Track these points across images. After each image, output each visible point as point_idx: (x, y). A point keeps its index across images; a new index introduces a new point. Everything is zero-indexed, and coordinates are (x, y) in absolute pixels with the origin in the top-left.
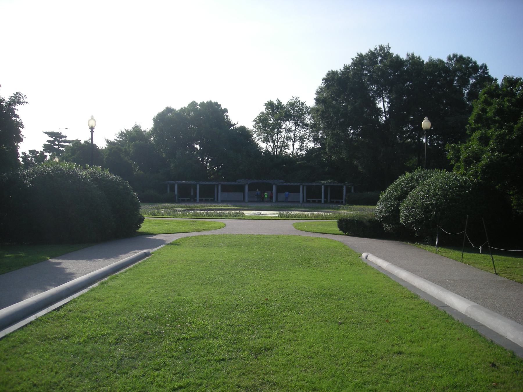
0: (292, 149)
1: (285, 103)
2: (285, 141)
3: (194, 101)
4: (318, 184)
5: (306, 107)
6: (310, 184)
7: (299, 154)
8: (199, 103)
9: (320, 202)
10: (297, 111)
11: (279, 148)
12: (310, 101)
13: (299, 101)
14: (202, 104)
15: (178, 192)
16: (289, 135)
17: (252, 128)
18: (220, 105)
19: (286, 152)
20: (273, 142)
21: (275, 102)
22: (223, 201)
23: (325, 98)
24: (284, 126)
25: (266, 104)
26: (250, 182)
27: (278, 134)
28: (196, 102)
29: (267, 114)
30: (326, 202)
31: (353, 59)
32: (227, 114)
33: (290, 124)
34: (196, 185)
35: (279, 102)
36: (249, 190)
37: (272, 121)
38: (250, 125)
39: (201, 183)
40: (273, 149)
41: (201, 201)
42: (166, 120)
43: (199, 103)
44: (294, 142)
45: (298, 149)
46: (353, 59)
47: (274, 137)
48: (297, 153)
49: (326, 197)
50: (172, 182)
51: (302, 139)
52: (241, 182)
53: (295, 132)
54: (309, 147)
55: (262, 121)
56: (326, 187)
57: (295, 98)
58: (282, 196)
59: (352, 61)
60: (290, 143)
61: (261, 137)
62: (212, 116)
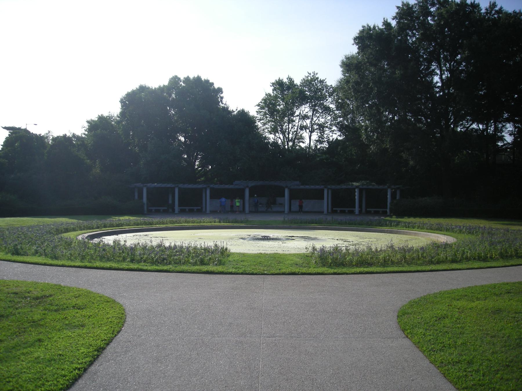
0: (309, 140)
1: (298, 81)
2: (299, 130)
3: (176, 76)
4: (350, 187)
5: (327, 86)
6: (338, 187)
7: (318, 147)
8: (182, 78)
9: (352, 212)
10: (315, 92)
11: (291, 140)
12: (332, 75)
13: (317, 78)
14: (187, 80)
15: (148, 199)
16: (305, 124)
17: (255, 115)
18: (213, 84)
19: (300, 146)
20: (283, 133)
21: (285, 80)
22: (213, 212)
23: (360, 63)
24: (297, 113)
25: (273, 84)
26: (252, 184)
27: (289, 123)
28: (179, 76)
29: (276, 97)
30: (360, 212)
31: (398, 7)
32: (222, 95)
33: (306, 109)
34: (173, 189)
35: (291, 80)
36: (211, 197)
37: (281, 107)
38: (253, 111)
39: (181, 186)
40: (283, 143)
41: (182, 212)
42: (137, 102)
43: (182, 78)
44: (311, 132)
45: (317, 141)
46: (398, 7)
47: (284, 127)
48: (316, 146)
49: (360, 206)
50: (139, 185)
51: (322, 127)
52: (237, 184)
53: (312, 119)
54: (331, 139)
55: (268, 104)
56: (361, 191)
57: (312, 74)
58: (296, 205)
59: (397, 10)
60: (305, 134)
61: (267, 126)
62: (200, 95)
